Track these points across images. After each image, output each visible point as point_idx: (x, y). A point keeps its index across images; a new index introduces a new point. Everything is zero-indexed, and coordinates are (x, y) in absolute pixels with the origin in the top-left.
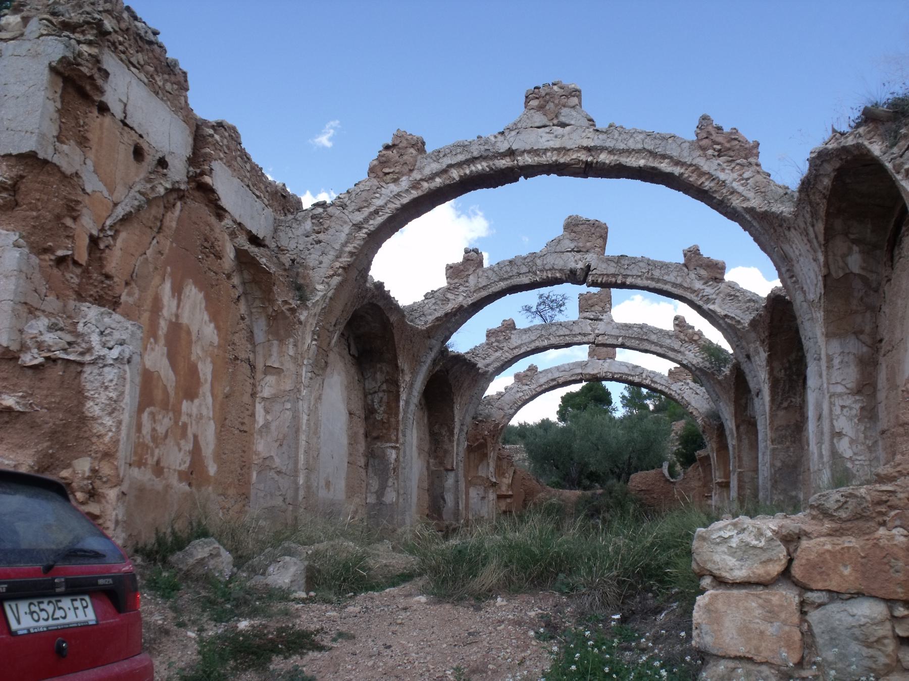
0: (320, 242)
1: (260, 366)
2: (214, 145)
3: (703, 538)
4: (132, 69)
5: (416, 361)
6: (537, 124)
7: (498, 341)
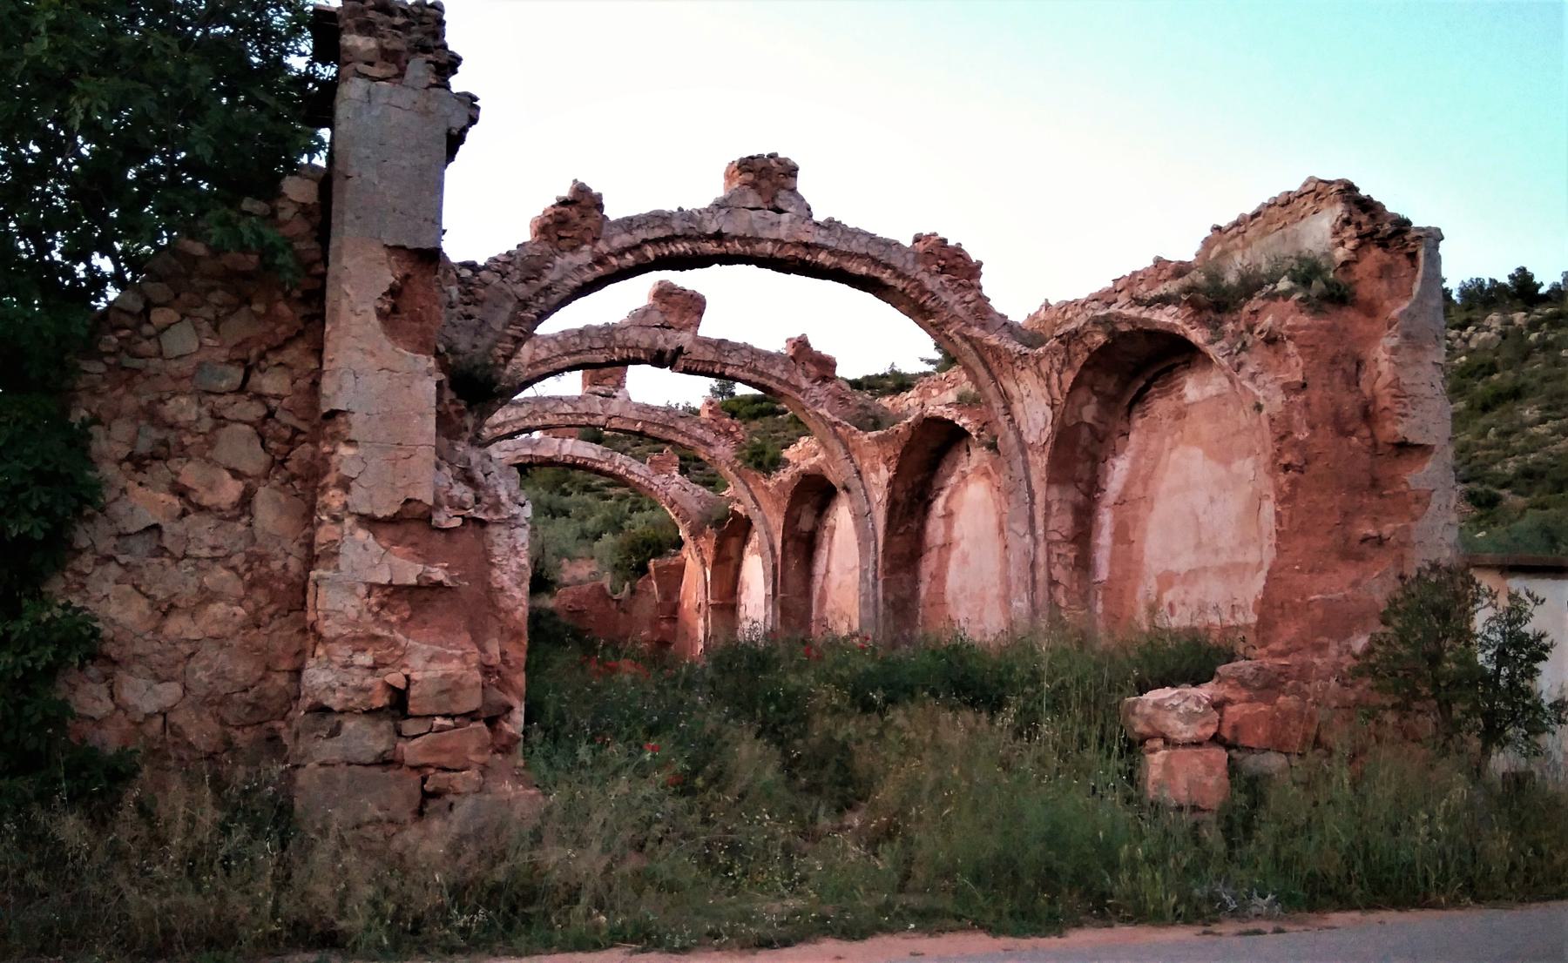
0: (470, 317)
6: (750, 205)
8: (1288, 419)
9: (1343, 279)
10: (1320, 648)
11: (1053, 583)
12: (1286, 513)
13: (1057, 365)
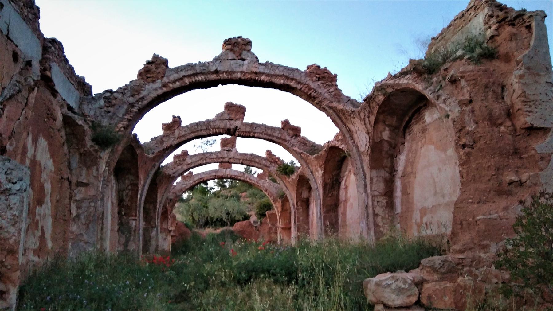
0: (109, 112)
1: (74, 181)
6: (230, 58)
7: (180, 161)
8: (462, 120)
9: (491, 46)
10: (485, 248)
11: (376, 215)
12: (464, 171)
13: (367, 114)
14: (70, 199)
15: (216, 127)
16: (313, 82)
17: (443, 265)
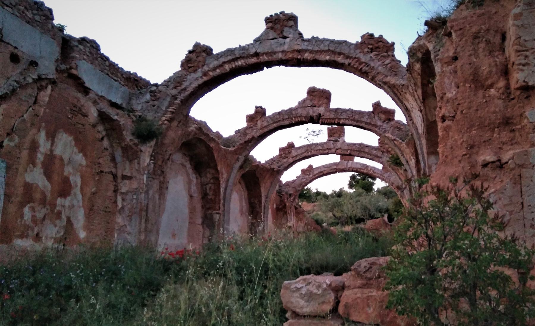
1: (119, 174)
2: (78, 51)
3: (287, 288)
4: (5, 7)
5: (230, 168)
6: (271, 38)
14: (116, 191)
15: (298, 115)
16: (364, 54)
17: (371, 267)
